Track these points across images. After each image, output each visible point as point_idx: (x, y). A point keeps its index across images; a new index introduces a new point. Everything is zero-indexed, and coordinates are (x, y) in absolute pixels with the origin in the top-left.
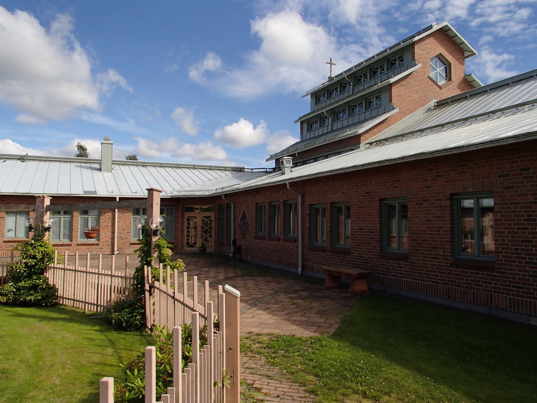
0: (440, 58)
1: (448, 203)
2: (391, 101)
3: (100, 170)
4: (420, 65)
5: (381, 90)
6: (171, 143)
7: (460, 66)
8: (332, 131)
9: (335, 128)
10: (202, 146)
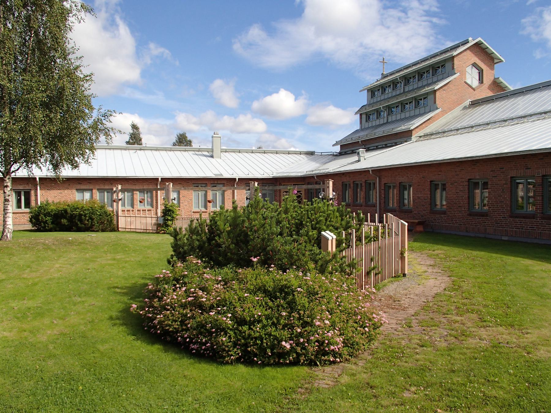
0: (475, 65)
1: (467, 183)
2: (435, 102)
3: (212, 157)
4: (458, 74)
5: (427, 94)
6: (209, 116)
7: (491, 71)
8: (387, 123)
9: (389, 121)
10: (242, 118)
